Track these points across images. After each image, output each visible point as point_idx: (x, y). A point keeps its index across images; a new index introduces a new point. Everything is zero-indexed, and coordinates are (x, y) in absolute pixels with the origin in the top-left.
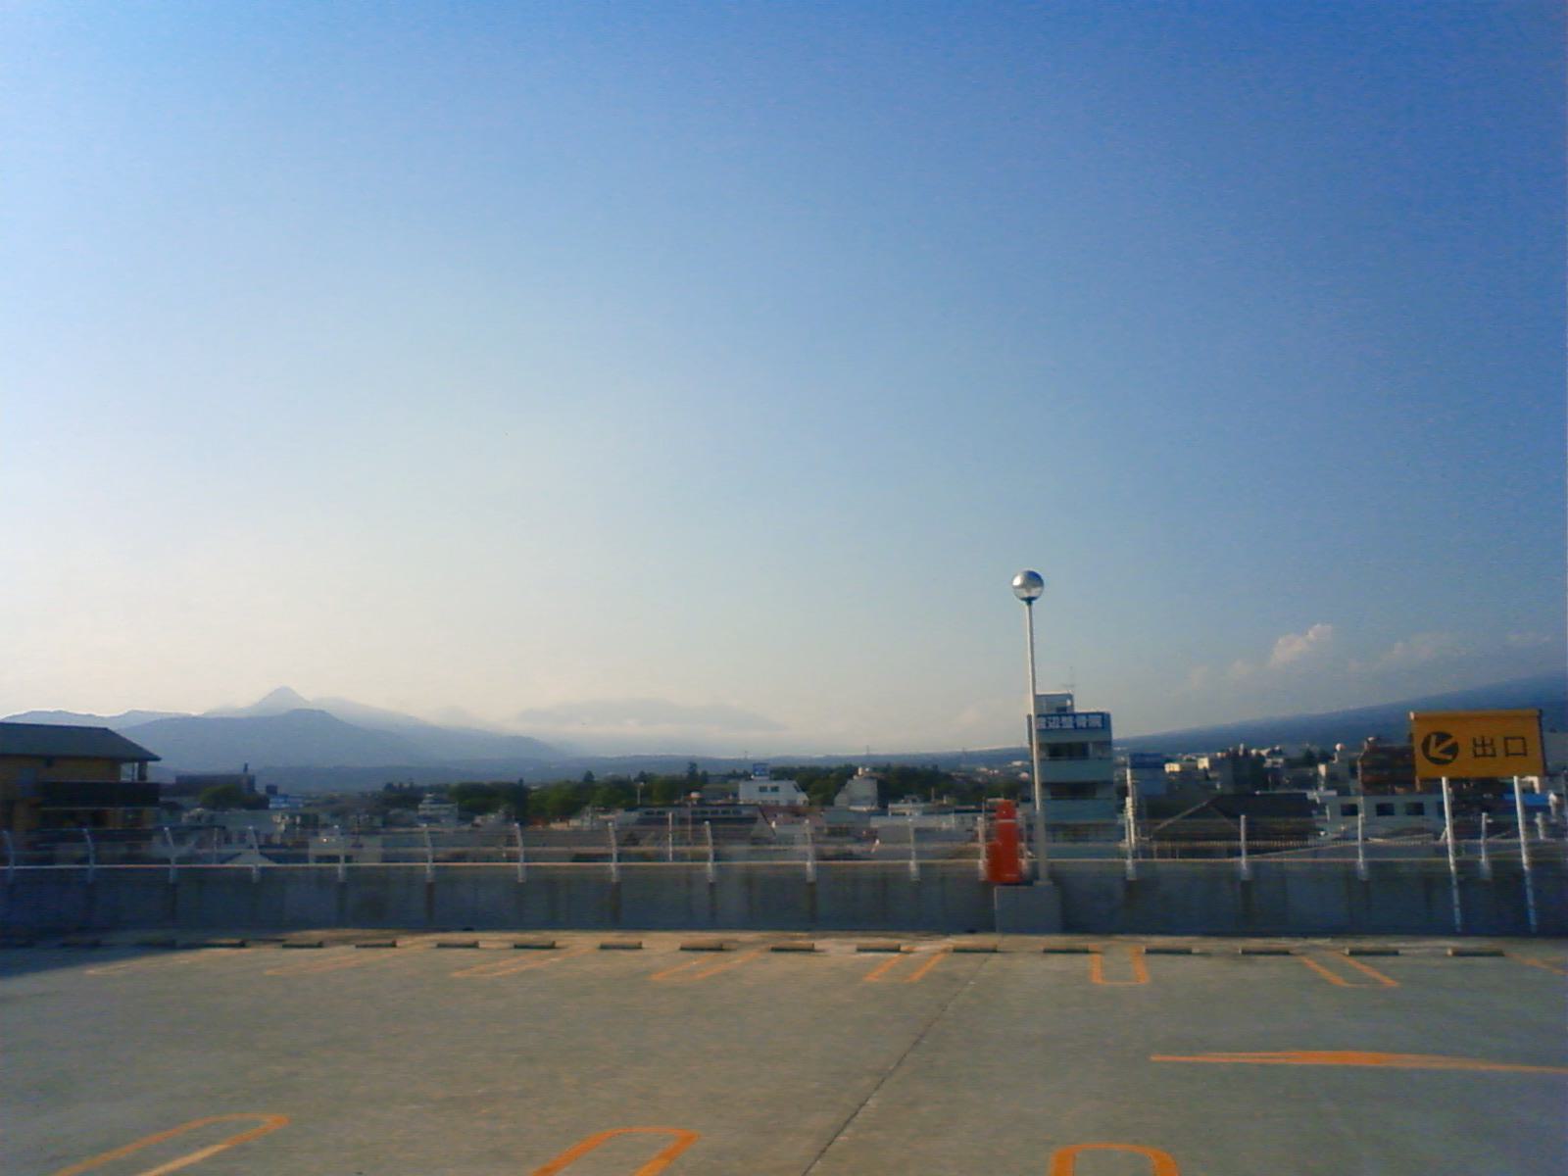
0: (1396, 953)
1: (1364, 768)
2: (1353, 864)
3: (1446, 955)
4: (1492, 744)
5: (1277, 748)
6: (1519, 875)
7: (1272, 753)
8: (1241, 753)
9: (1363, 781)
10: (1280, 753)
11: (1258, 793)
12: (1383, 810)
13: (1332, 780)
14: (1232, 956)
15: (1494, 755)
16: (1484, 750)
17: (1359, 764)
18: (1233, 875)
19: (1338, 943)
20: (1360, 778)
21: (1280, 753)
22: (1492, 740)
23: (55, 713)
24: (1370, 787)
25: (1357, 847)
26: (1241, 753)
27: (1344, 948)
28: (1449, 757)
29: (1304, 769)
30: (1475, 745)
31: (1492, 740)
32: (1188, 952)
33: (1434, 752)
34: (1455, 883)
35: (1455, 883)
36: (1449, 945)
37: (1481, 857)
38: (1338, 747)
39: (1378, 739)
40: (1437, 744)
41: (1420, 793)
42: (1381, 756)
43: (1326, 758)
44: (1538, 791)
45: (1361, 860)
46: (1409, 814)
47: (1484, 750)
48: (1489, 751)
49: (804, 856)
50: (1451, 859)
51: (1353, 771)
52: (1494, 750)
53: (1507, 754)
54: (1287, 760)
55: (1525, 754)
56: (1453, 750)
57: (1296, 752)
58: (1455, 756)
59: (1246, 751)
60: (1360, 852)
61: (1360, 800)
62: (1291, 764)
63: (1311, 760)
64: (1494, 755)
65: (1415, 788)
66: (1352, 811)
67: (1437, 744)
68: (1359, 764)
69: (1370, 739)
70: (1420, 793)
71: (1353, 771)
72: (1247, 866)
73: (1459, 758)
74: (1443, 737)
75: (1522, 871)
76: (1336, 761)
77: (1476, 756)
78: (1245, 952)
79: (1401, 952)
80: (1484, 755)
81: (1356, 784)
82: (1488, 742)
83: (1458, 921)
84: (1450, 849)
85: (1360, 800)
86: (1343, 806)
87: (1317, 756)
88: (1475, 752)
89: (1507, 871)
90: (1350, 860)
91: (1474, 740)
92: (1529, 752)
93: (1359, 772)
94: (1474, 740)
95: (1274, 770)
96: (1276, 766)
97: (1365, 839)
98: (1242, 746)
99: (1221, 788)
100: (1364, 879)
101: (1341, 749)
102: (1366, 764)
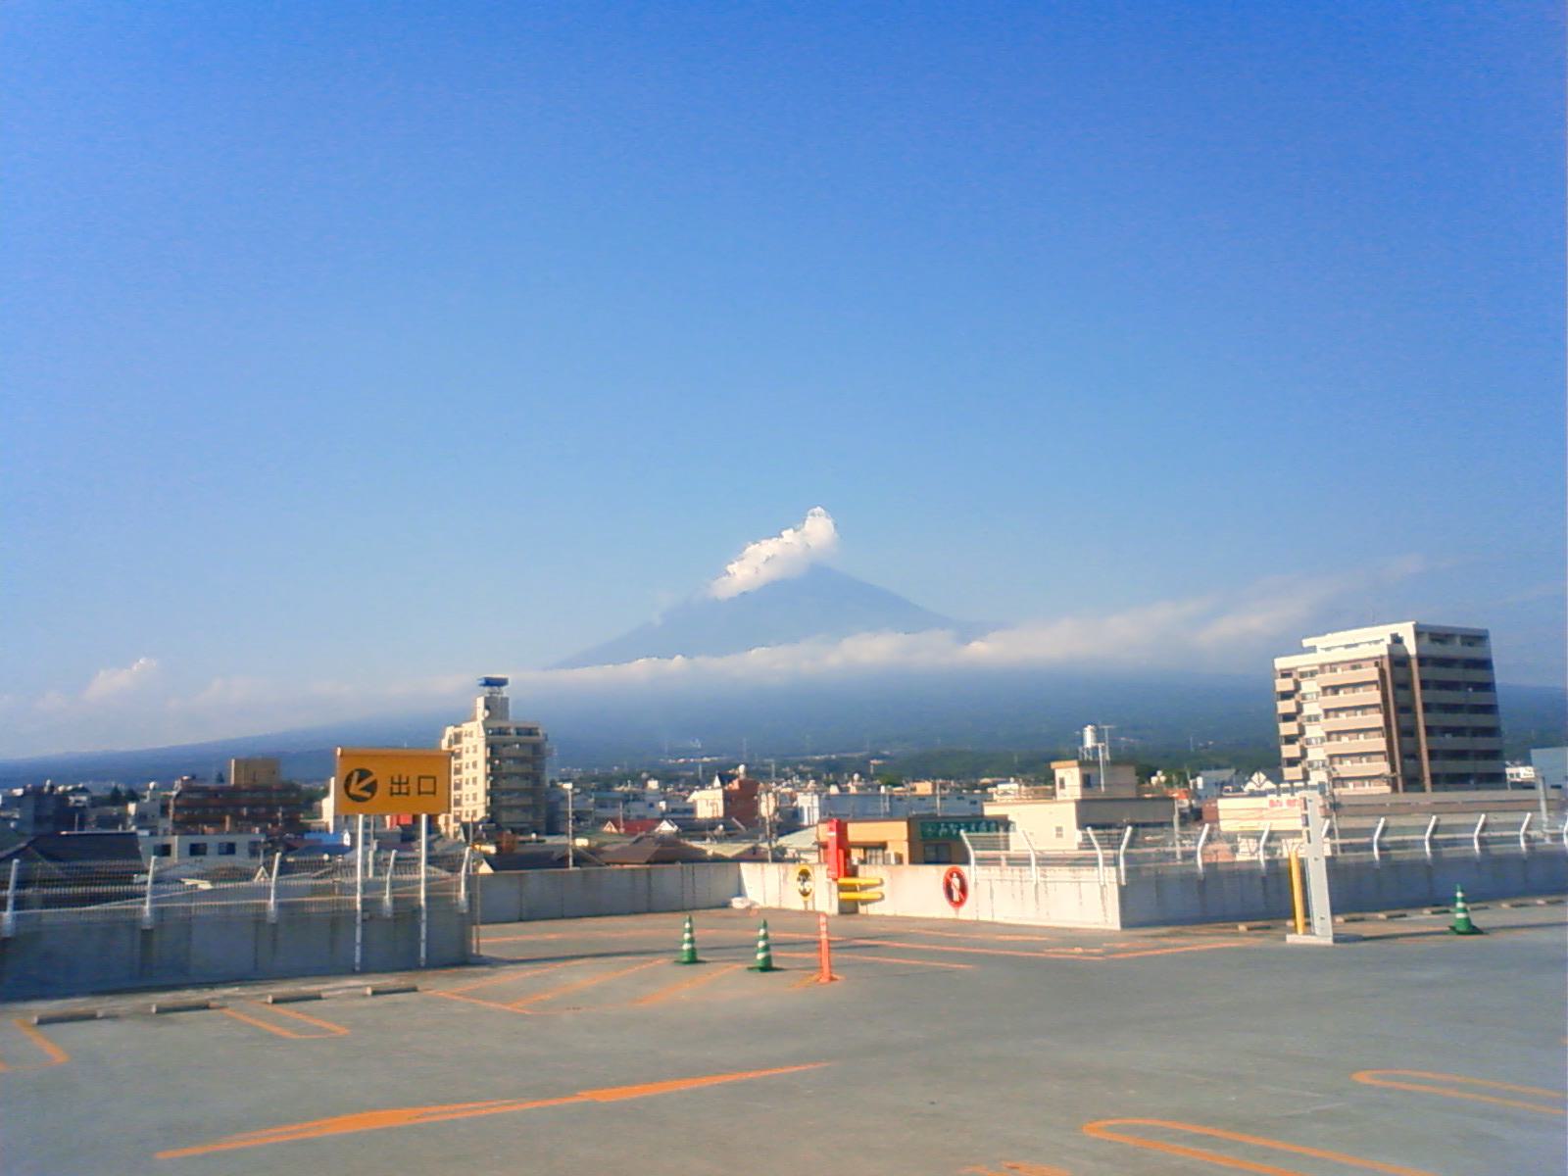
0: (318, 997)
1: (177, 807)
2: (264, 906)
3: (365, 996)
4: (407, 783)
5: (81, 786)
6: (417, 910)
7: (76, 791)
8: (46, 790)
9: (174, 821)
10: (84, 790)
11: (64, 833)
12: (196, 850)
13: (141, 818)
14: (143, 1014)
15: (407, 794)
16: (400, 789)
17: (172, 802)
18: (133, 923)
19: (258, 990)
20: (171, 818)
21: (84, 790)
22: (408, 779)
23: (1324, 634)
24: (181, 826)
25: (6, 897)
26: (46, 790)
27: (266, 995)
28: (367, 794)
29: (108, 808)
30: (393, 783)
31: (408, 779)
32: (92, 1017)
33: (354, 789)
34: (359, 920)
35: (359, 920)
36: (366, 984)
37: (385, 894)
38: (152, 785)
39: (194, 777)
40: (360, 780)
41: (228, 833)
42: (195, 796)
43: (134, 796)
44: (331, 831)
45: (147, 907)
46: (221, 853)
47: (400, 789)
48: (404, 790)
49: (264, 892)
50: (358, 898)
51: (164, 810)
52: (408, 789)
53: (420, 793)
54: (93, 798)
55: (434, 793)
56: (372, 788)
57: (101, 790)
58: (373, 794)
59: (52, 788)
60: (273, 891)
61: (175, 841)
62: (95, 802)
63: (118, 799)
64: (407, 794)
65: (224, 826)
66: (165, 850)
67: (360, 780)
68: (172, 802)
69: (185, 778)
70: (228, 833)
71: (164, 810)
72: (275, 907)
73: (377, 795)
74: (364, 774)
75: (420, 906)
76: (147, 801)
77: (392, 794)
78: (161, 1011)
79: (324, 995)
80: (400, 793)
81: (166, 823)
82: (404, 780)
83: (357, 960)
84: (359, 887)
85: (175, 841)
86: (220, 845)
87: (124, 794)
88: (392, 789)
89: (406, 910)
90: (263, 901)
91: (392, 779)
92: (437, 793)
93: (171, 811)
94: (392, 779)
95: (81, 810)
96: (78, 805)
97: (1528, 828)
98: (48, 782)
99: (1106, 792)
100: (274, 921)
101: (154, 789)
102: (178, 802)
